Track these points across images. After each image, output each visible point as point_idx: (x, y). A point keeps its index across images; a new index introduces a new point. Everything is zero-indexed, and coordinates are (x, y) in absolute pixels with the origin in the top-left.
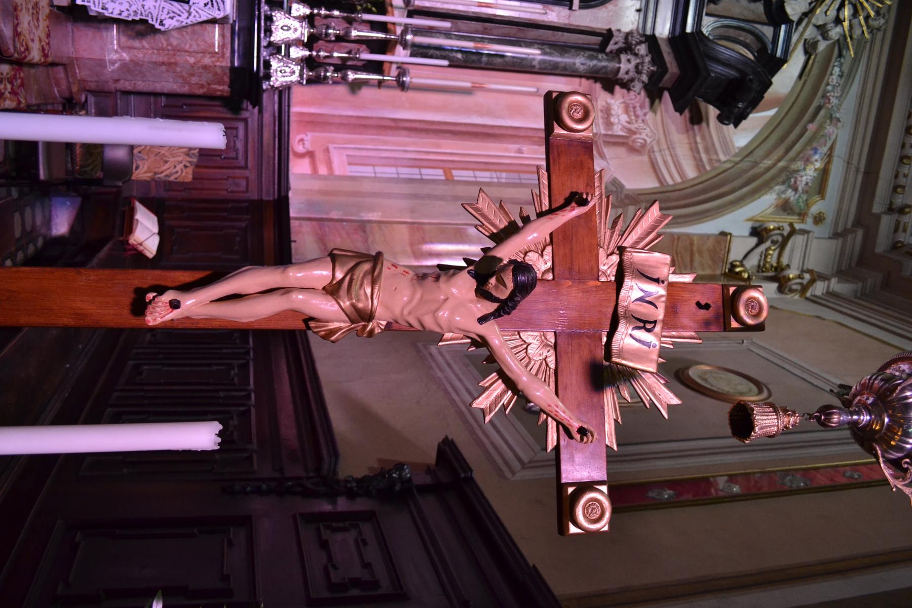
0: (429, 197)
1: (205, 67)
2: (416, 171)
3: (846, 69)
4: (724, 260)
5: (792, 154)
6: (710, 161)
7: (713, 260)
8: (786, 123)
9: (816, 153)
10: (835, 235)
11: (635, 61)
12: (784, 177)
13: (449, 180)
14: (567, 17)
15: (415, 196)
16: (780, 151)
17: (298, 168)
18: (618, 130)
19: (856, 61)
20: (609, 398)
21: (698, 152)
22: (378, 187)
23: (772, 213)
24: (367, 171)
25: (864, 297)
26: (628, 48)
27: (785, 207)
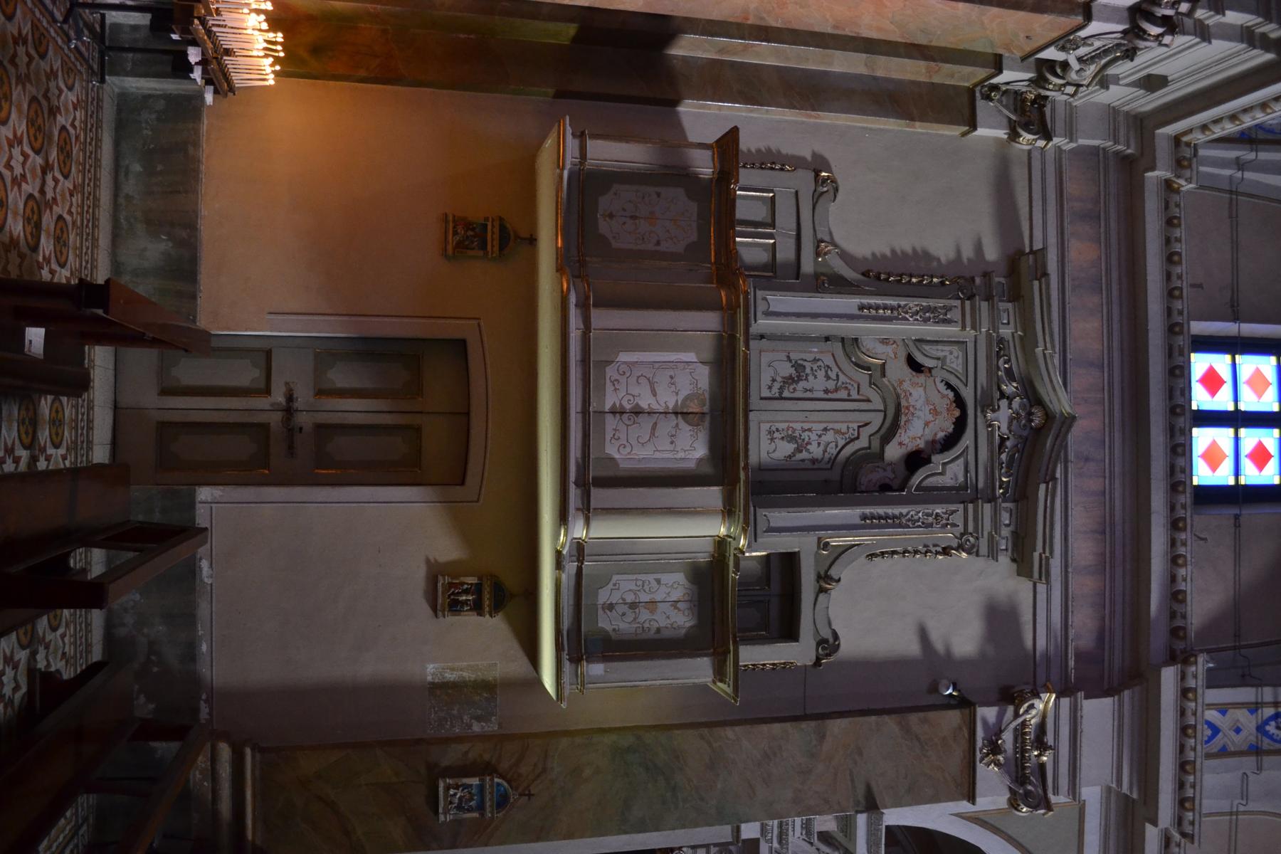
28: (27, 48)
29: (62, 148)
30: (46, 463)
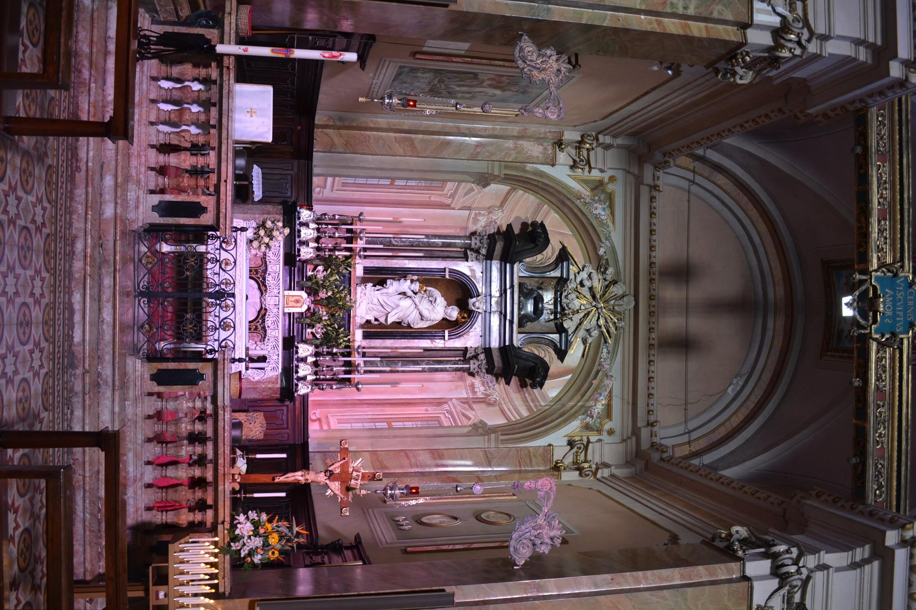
0: (381, 437)
1: (270, 388)
2: (373, 424)
3: (611, 349)
4: (551, 461)
5: (586, 397)
6: (536, 406)
7: (543, 460)
8: (579, 382)
9: (601, 396)
10: (624, 441)
11: (477, 364)
12: (583, 411)
13: (390, 428)
15: (373, 437)
16: (578, 396)
17: (313, 427)
18: (479, 395)
19: (616, 342)
20: (350, 493)
21: (528, 402)
22: (353, 434)
23: (580, 431)
24: (348, 426)
25: (635, 479)
26: (475, 357)
27: (587, 427)
28: (16, 516)
29: (30, 20)
30: (41, 283)
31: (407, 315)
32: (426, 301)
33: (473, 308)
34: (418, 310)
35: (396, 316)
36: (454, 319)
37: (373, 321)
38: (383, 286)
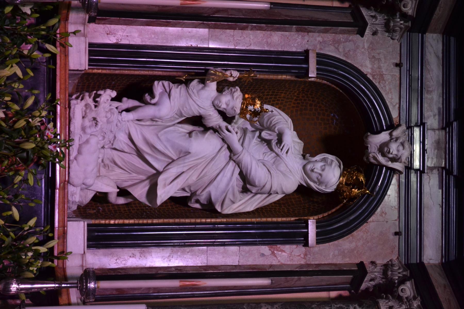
14: (302, 256)
31: (206, 180)
32: (255, 140)
33: (382, 160)
34: (238, 164)
35: (179, 183)
36: (330, 190)
37: (113, 198)
38: (141, 99)
